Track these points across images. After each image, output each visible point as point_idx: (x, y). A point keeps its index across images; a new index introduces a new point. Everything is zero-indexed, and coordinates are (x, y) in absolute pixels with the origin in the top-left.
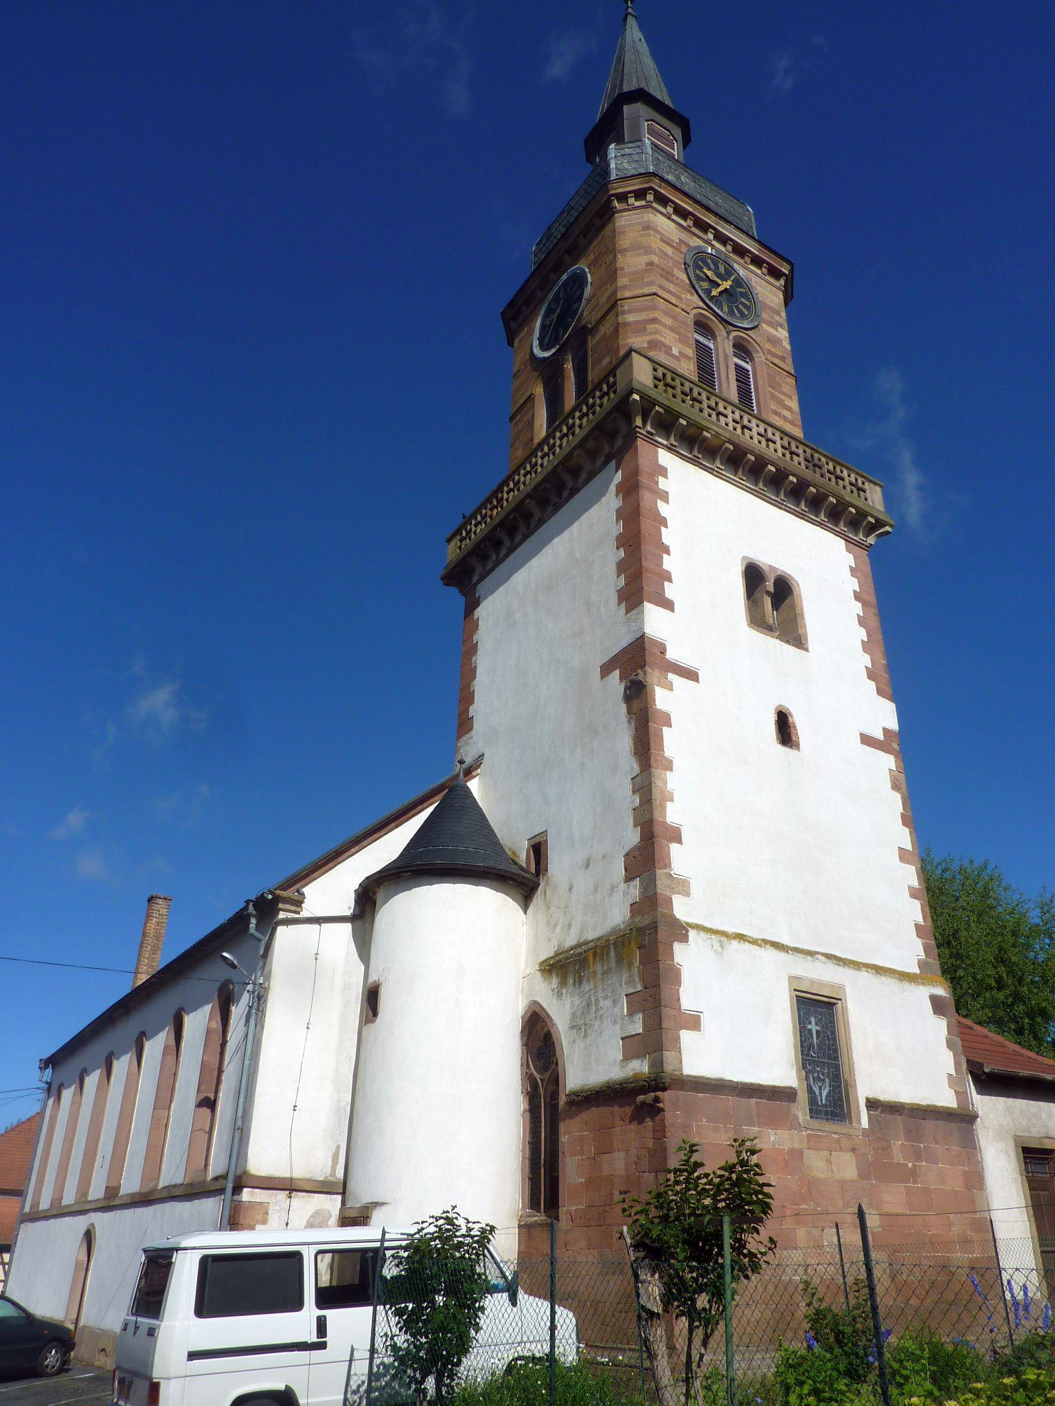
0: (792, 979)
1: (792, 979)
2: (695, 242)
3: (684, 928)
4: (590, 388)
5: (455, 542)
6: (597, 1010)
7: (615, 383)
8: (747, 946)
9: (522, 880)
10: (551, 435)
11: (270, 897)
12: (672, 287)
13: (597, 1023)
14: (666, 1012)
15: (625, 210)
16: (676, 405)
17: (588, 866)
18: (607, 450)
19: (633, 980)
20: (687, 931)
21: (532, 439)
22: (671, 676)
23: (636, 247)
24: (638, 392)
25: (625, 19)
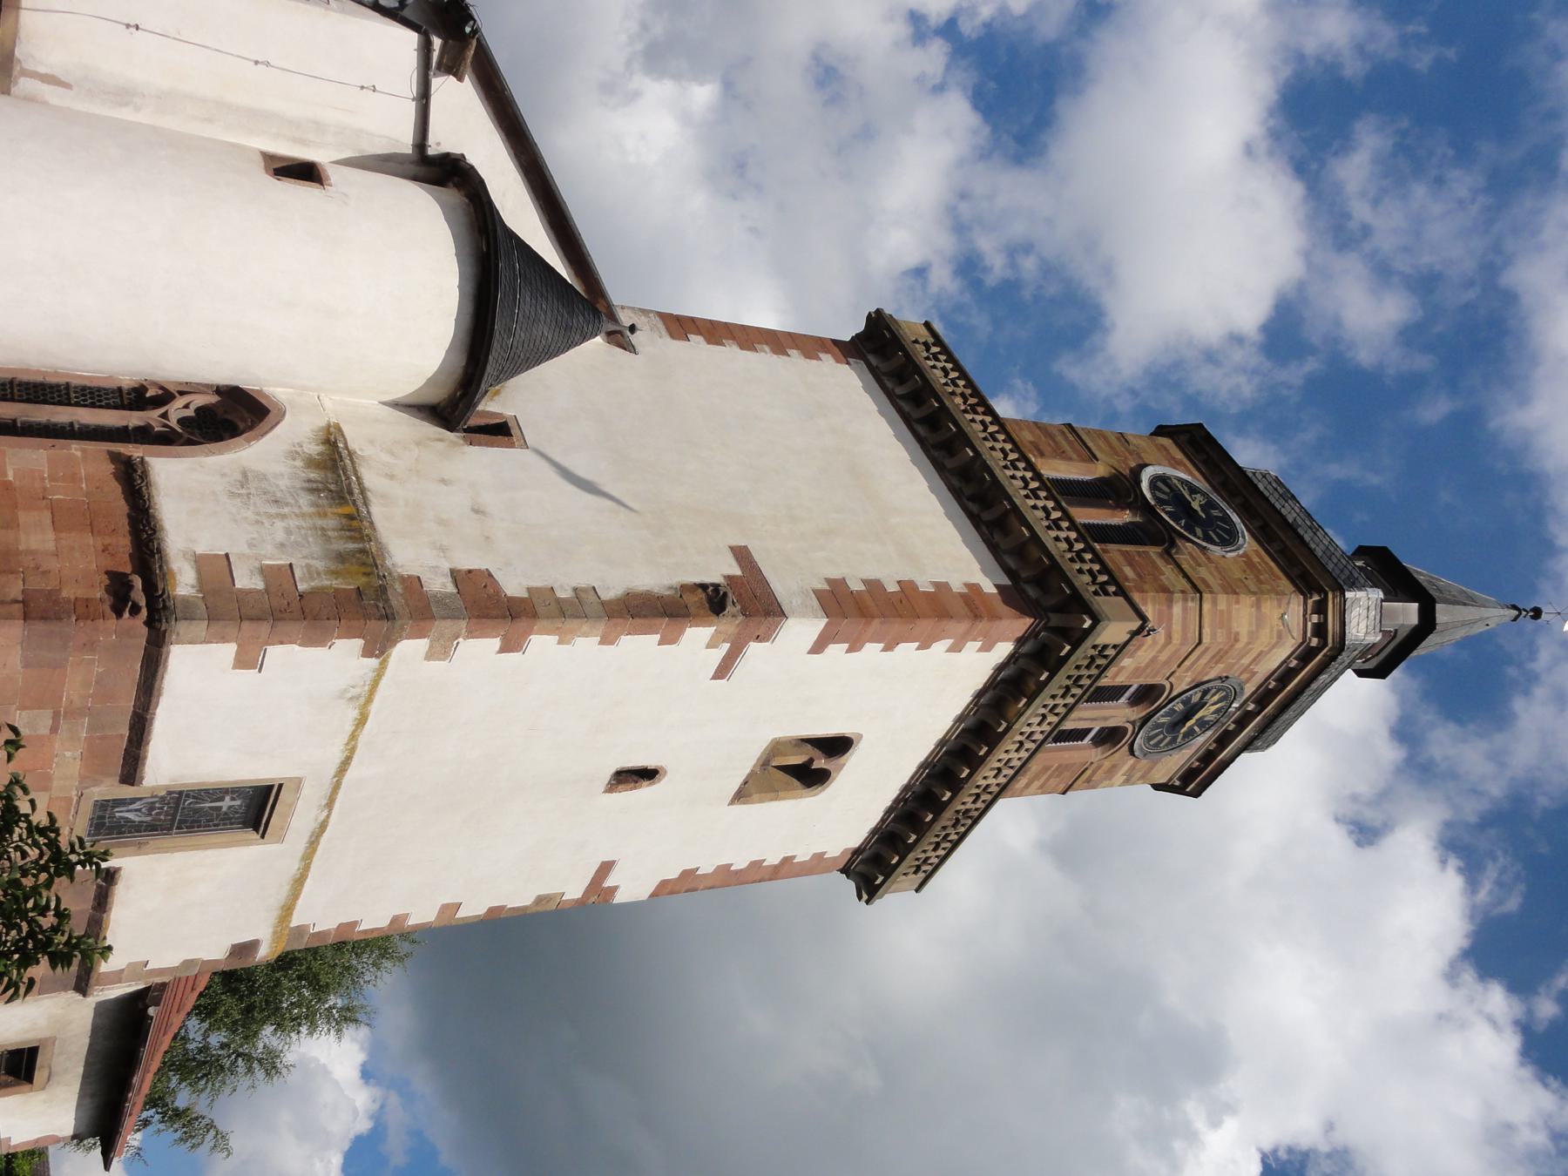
0: (298, 783)
1: (298, 783)
2: (1249, 689)
3: (382, 653)
4: (1097, 546)
5: (924, 335)
6: (270, 516)
7: (1106, 593)
8: (349, 728)
9: (457, 406)
10: (1073, 526)
11: (468, 30)
12: (1203, 661)
13: (250, 514)
14: (265, 628)
15: (1305, 611)
16: (1068, 669)
17: (477, 511)
18: (1024, 575)
19: (312, 579)
20: (377, 657)
21: (1042, 454)
22: (726, 646)
23: (1260, 621)
24: (1093, 627)
25: (1514, 607)
